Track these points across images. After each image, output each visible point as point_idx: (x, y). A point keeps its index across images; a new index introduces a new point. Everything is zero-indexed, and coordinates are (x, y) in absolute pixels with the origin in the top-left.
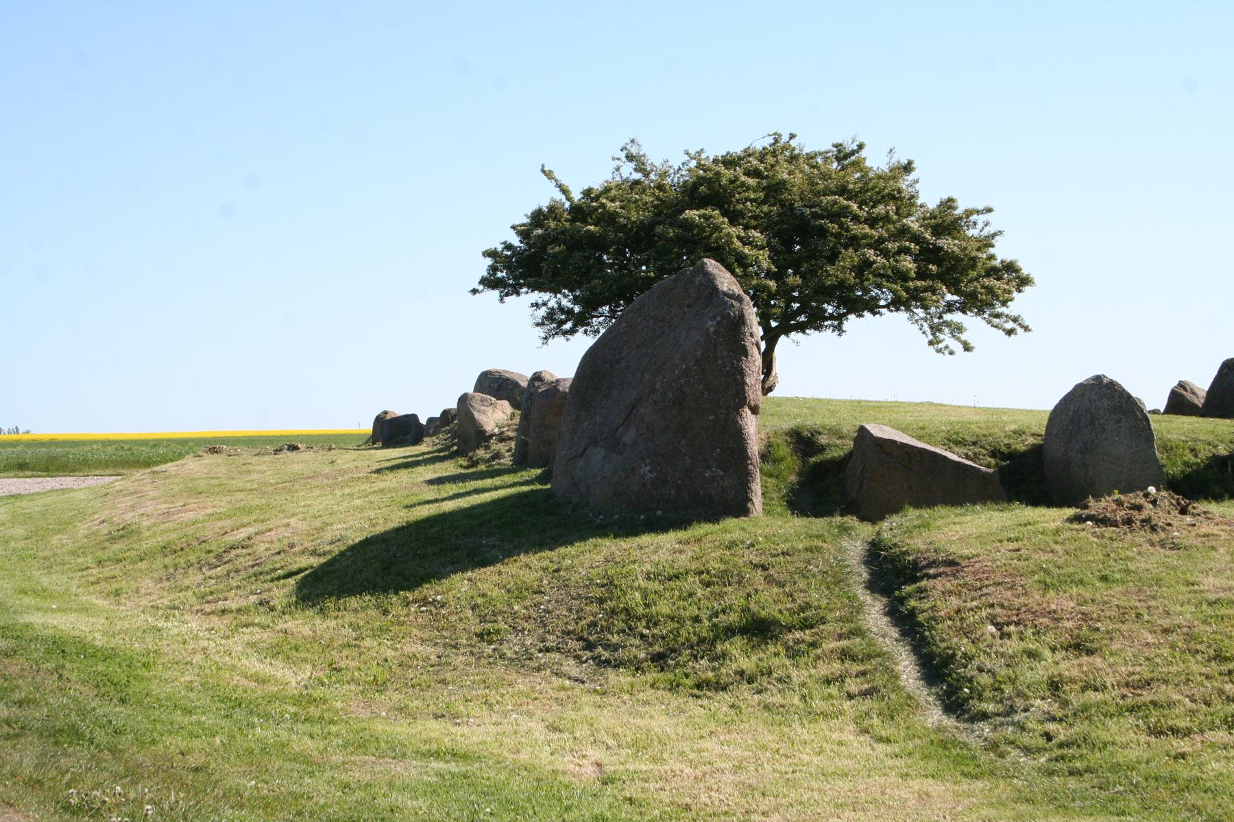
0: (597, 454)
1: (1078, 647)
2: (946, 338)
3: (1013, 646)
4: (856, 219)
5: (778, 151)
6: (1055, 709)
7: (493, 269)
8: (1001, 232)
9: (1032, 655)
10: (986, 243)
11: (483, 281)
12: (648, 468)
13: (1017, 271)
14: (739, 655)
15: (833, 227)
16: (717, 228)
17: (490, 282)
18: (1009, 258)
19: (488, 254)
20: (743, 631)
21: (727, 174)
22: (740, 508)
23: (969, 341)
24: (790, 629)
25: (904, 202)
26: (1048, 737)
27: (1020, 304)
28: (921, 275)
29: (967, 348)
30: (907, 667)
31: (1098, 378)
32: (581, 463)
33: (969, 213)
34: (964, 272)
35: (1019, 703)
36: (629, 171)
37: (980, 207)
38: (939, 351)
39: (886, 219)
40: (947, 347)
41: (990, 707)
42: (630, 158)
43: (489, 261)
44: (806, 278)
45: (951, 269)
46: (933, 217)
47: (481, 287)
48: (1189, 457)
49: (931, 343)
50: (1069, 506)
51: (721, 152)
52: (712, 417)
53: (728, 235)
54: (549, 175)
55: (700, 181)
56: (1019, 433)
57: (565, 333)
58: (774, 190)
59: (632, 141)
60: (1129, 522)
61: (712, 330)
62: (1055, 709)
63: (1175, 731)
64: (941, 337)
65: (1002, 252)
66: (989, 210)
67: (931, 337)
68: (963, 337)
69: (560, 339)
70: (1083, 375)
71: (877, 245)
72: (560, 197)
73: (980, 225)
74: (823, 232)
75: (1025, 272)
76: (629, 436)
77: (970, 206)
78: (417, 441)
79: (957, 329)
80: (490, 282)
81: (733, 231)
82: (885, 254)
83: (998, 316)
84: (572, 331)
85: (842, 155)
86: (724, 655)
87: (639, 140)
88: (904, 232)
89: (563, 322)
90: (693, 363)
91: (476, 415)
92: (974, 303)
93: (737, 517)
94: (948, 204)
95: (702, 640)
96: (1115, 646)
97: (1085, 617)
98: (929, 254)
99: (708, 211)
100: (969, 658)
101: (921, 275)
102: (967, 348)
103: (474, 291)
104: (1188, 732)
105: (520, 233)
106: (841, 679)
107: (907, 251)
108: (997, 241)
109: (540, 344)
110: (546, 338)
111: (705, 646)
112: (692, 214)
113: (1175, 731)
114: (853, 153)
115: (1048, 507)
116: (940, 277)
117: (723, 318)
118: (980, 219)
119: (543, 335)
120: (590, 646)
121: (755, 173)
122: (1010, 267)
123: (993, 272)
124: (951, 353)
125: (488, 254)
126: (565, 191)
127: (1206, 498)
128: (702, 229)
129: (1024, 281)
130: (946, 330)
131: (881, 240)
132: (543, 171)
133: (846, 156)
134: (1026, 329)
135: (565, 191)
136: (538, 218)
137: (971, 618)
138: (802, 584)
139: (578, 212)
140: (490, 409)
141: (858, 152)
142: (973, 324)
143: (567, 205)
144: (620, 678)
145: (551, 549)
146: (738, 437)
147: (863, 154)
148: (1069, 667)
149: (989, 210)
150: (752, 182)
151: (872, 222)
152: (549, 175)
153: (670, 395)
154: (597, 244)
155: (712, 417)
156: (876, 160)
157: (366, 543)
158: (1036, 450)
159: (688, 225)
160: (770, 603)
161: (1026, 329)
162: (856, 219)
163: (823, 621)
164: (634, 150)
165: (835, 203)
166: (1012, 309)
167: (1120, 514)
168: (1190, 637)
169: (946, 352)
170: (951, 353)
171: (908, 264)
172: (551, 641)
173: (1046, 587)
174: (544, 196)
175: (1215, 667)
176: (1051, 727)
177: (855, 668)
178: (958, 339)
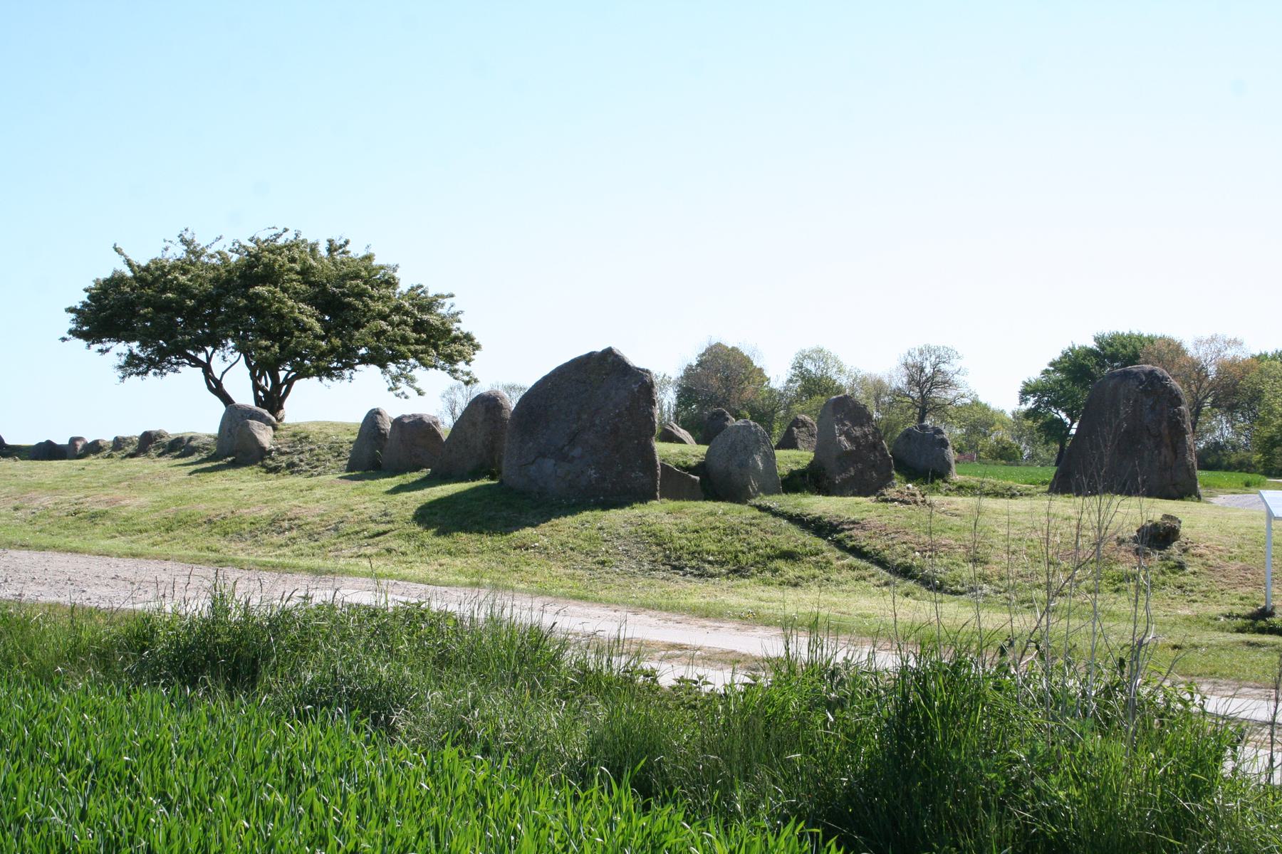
0: (549, 464)
2: (403, 385)
4: (371, 297)
8: (462, 312)
11: (71, 332)
12: (593, 471)
14: (790, 571)
29: (420, 393)
32: (533, 468)
37: (446, 294)
38: (397, 395)
40: (403, 393)
43: (73, 316)
47: (68, 336)
50: (1128, 489)
52: (636, 442)
58: (305, 272)
61: (636, 390)
65: (464, 326)
66: (452, 296)
67: (392, 385)
68: (417, 385)
73: (447, 306)
77: (439, 292)
80: (75, 333)
84: (145, 373)
90: (624, 409)
102: (420, 393)
103: (64, 339)
107: (405, 323)
109: (118, 382)
110: (124, 377)
115: (675, 500)
117: (643, 383)
118: (448, 302)
119: (122, 375)
122: (468, 337)
123: (456, 339)
126: (129, 264)
130: (403, 380)
132: (116, 250)
135: (129, 264)
140: (264, 432)
141: (344, 246)
145: (533, 526)
147: (348, 248)
153: (608, 428)
155: (636, 442)
164: (188, 236)
165: (357, 286)
169: (403, 397)
170: (406, 397)
178: (412, 387)
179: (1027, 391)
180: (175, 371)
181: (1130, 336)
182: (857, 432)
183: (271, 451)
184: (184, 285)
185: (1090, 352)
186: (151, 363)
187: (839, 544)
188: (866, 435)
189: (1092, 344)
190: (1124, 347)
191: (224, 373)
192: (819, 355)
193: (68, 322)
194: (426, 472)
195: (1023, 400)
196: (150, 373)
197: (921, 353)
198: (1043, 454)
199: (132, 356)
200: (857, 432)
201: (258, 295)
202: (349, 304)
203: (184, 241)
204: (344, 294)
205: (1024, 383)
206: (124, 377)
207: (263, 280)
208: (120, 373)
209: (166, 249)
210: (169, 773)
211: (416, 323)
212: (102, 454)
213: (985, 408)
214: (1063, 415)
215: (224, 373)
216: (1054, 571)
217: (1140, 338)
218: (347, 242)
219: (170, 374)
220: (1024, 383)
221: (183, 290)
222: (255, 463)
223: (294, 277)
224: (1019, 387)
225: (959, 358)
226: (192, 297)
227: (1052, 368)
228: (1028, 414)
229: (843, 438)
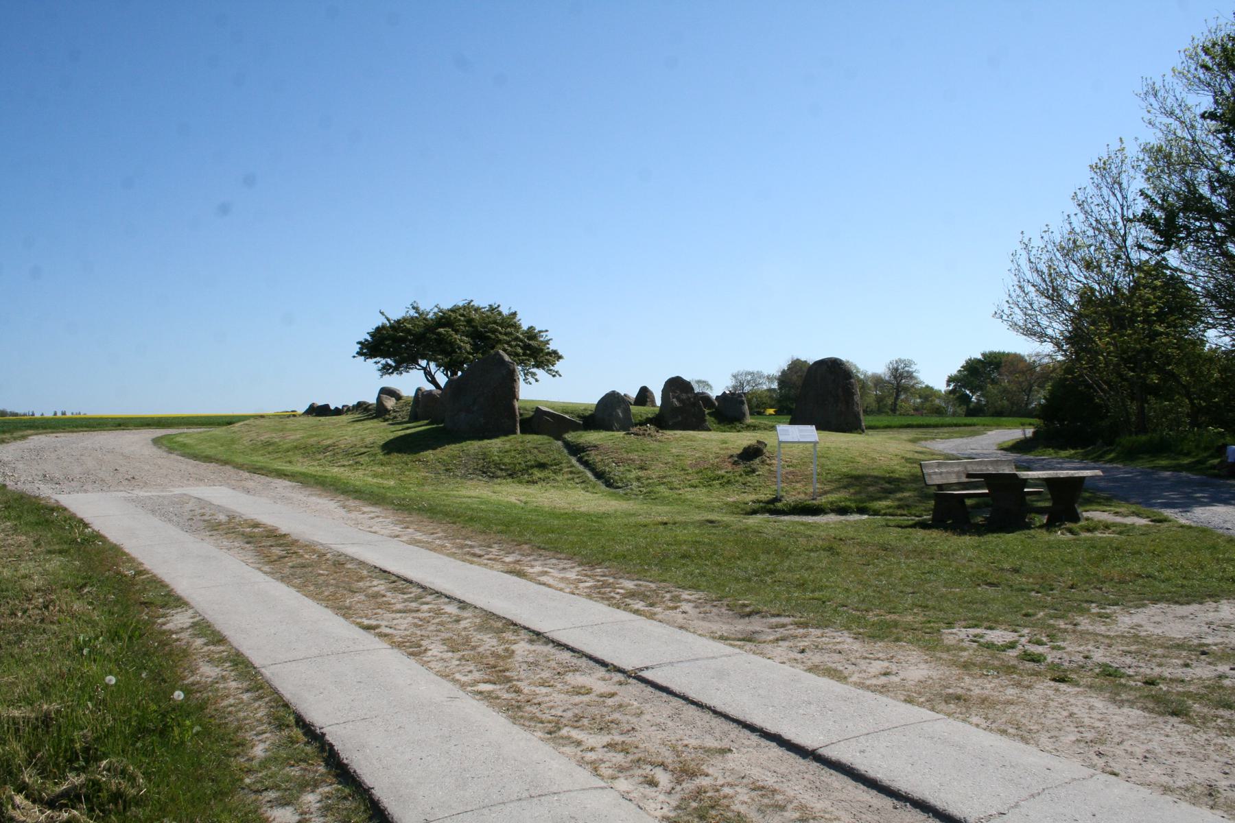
1: (642, 468)
3: (621, 469)
4: (500, 333)
5: (468, 307)
6: (640, 484)
7: (361, 349)
9: (629, 471)
10: (547, 342)
11: (358, 353)
13: (557, 354)
14: (537, 474)
15: (493, 336)
16: (451, 336)
17: (360, 354)
18: (555, 349)
20: (536, 467)
21: (453, 315)
22: (515, 433)
24: (552, 465)
25: (516, 327)
26: (641, 491)
27: (558, 366)
28: (524, 354)
29: (537, 381)
30: (589, 474)
31: (614, 392)
33: (540, 332)
34: (538, 354)
35: (629, 484)
36: (412, 313)
39: (511, 334)
41: (620, 484)
42: (414, 308)
43: (359, 346)
44: (542, 362)
45: (534, 352)
46: (526, 333)
48: (640, 418)
51: (450, 306)
53: (455, 339)
54: (382, 313)
55: (442, 317)
56: (585, 410)
57: (389, 374)
58: (470, 321)
60: (644, 434)
62: (640, 484)
63: (676, 489)
65: (552, 346)
66: (547, 331)
69: (387, 376)
70: (608, 391)
71: (508, 343)
72: (387, 322)
74: (489, 338)
75: (560, 354)
79: (533, 374)
80: (360, 354)
81: (458, 337)
82: (511, 346)
83: (551, 370)
84: (392, 373)
85: (492, 309)
86: (532, 473)
87: (417, 301)
88: (517, 339)
89: (389, 369)
92: (539, 365)
94: (531, 329)
95: (524, 470)
96: (653, 468)
97: (642, 460)
98: (526, 347)
99: (447, 329)
100: (610, 472)
101: (524, 354)
102: (537, 381)
103: (354, 357)
104: (680, 489)
105: (371, 336)
106: (573, 479)
107: (519, 345)
108: (551, 342)
111: (525, 471)
112: (441, 330)
113: (676, 489)
116: (530, 355)
118: (544, 334)
120: (484, 473)
121: (462, 315)
122: (555, 352)
123: (549, 354)
125: (359, 343)
126: (388, 320)
127: (1031, 367)
128: (445, 335)
129: (560, 357)
131: (510, 341)
133: (493, 310)
134: (560, 376)
135: (388, 320)
136: (378, 329)
137: (607, 462)
138: (551, 453)
139: (392, 327)
142: (540, 373)
143: (388, 325)
144: (499, 481)
146: (513, 407)
148: (640, 473)
149: (547, 331)
150: (462, 318)
151: (506, 334)
152: (382, 313)
154: (403, 340)
156: (505, 311)
158: (592, 416)
159: (439, 334)
160: (542, 458)
161: (560, 376)
162: (500, 333)
163: (561, 463)
164: (415, 305)
166: (556, 368)
167: (641, 432)
168: (673, 464)
171: (520, 351)
172: (470, 471)
173: (628, 453)
174: (380, 321)
175: (682, 473)
176: (641, 489)
177: (576, 476)
179: (950, 380)
180: (408, 372)
181: (999, 353)
182: (684, 396)
185: (979, 361)
186: (396, 369)
187: (580, 460)
188: (689, 398)
189: (980, 357)
190: (996, 358)
192: (908, 363)
193: (357, 348)
194: (426, 422)
195: (948, 385)
197: (897, 362)
198: (959, 410)
199: (387, 364)
200: (684, 396)
202: (488, 336)
204: (486, 332)
207: (443, 326)
208: (380, 373)
210: (1006, 566)
211: (525, 345)
213: (932, 389)
214: (968, 392)
216: (491, 472)
217: (1003, 354)
218: (499, 306)
219: (404, 374)
221: (408, 331)
223: (462, 323)
224: (946, 378)
226: (411, 334)
228: (951, 392)
229: (674, 400)
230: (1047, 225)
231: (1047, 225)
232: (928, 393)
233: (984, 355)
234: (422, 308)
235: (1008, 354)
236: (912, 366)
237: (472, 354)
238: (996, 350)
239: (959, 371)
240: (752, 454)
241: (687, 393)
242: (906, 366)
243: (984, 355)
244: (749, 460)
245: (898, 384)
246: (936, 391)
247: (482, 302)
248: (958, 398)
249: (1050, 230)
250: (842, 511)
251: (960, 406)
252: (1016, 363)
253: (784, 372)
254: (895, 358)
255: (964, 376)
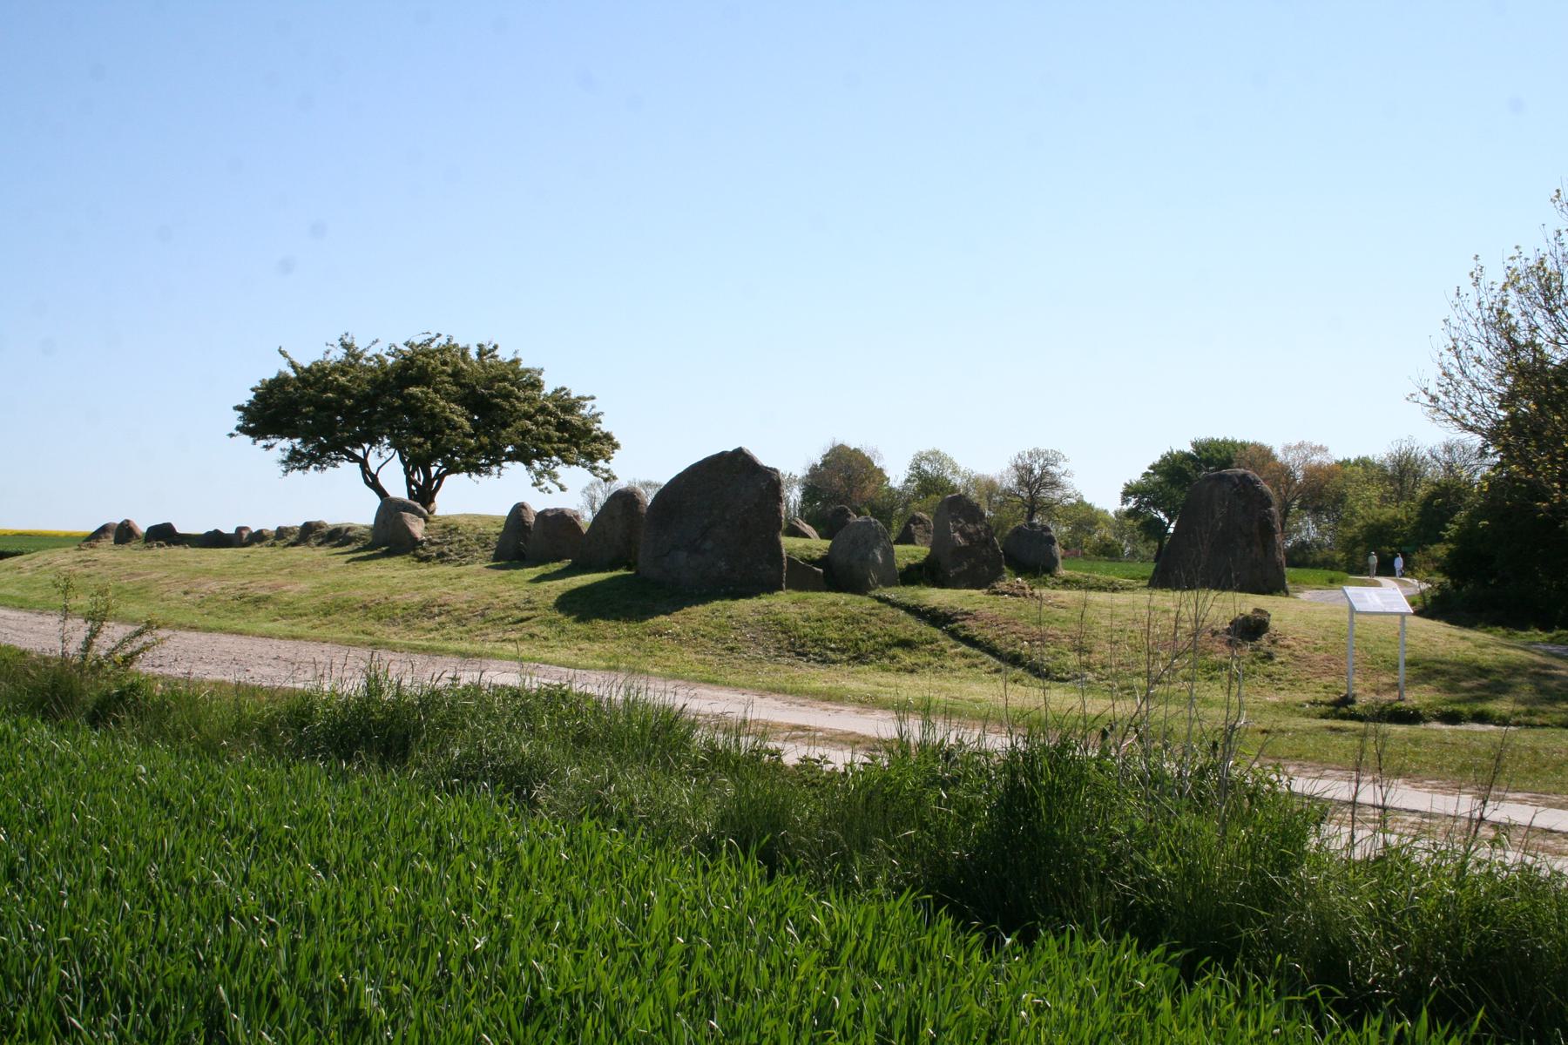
4: (518, 398)
11: (238, 428)
19: (238, 408)
23: (564, 484)
28: (561, 440)
29: (562, 489)
37: (587, 396)
38: (541, 490)
43: (240, 413)
47: (235, 432)
49: (534, 485)
58: (457, 375)
59: (347, 334)
64: (542, 480)
65: (605, 426)
66: (593, 398)
68: (559, 481)
73: (588, 407)
76: (708, 545)
77: (581, 394)
78: (348, 543)
84: (307, 468)
91: (411, 528)
93: (560, 597)
102: (562, 489)
103: (232, 435)
107: (549, 423)
114: (490, 351)
118: (589, 404)
122: (608, 437)
123: (596, 439)
124: (550, 492)
130: (546, 476)
135: (293, 366)
147: (496, 353)
149: (593, 398)
154: (337, 407)
157: (1224, 589)
164: (348, 340)
170: (550, 492)
179: (1129, 492)
180: (335, 466)
181: (1225, 442)
182: (971, 529)
183: (422, 542)
184: (344, 385)
185: (1187, 457)
186: (312, 459)
187: (953, 634)
188: (978, 532)
189: (1188, 449)
190: (1219, 452)
191: (379, 468)
192: (935, 456)
193: (235, 419)
195: (1125, 501)
196: (311, 468)
197: (1030, 455)
198: (1143, 550)
200: (971, 529)
201: (412, 396)
202: (497, 405)
203: (344, 345)
204: (492, 396)
205: (1126, 484)
206: (287, 471)
207: (416, 381)
208: (283, 468)
209: (328, 353)
211: (559, 423)
212: (266, 543)
213: (1089, 507)
214: (1162, 515)
215: (379, 468)
219: (330, 469)
220: (1126, 484)
221: (343, 391)
222: (408, 553)
224: (1121, 488)
225: (1066, 460)
226: (351, 397)
227: (1152, 471)
228: (1131, 514)
229: (957, 534)
230: (1517, 247)
231: (1517, 247)
232: (1085, 519)
233: (1194, 445)
234: (360, 345)
235: (1244, 446)
236: (1060, 464)
237: (471, 436)
238: (1219, 435)
239: (1146, 474)
240: (1251, 629)
241: (975, 523)
242: (1048, 462)
243: (1194, 445)
244: (1254, 639)
245: (1032, 497)
246: (1098, 512)
247: (468, 338)
248: (1142, 524)
249: (1524, 255)
250: (1452, 718)
251: (1146, 541)
252: (1259, 461)
253: (814, 471)
254: (1027, 446)
255: (1158, 484)
